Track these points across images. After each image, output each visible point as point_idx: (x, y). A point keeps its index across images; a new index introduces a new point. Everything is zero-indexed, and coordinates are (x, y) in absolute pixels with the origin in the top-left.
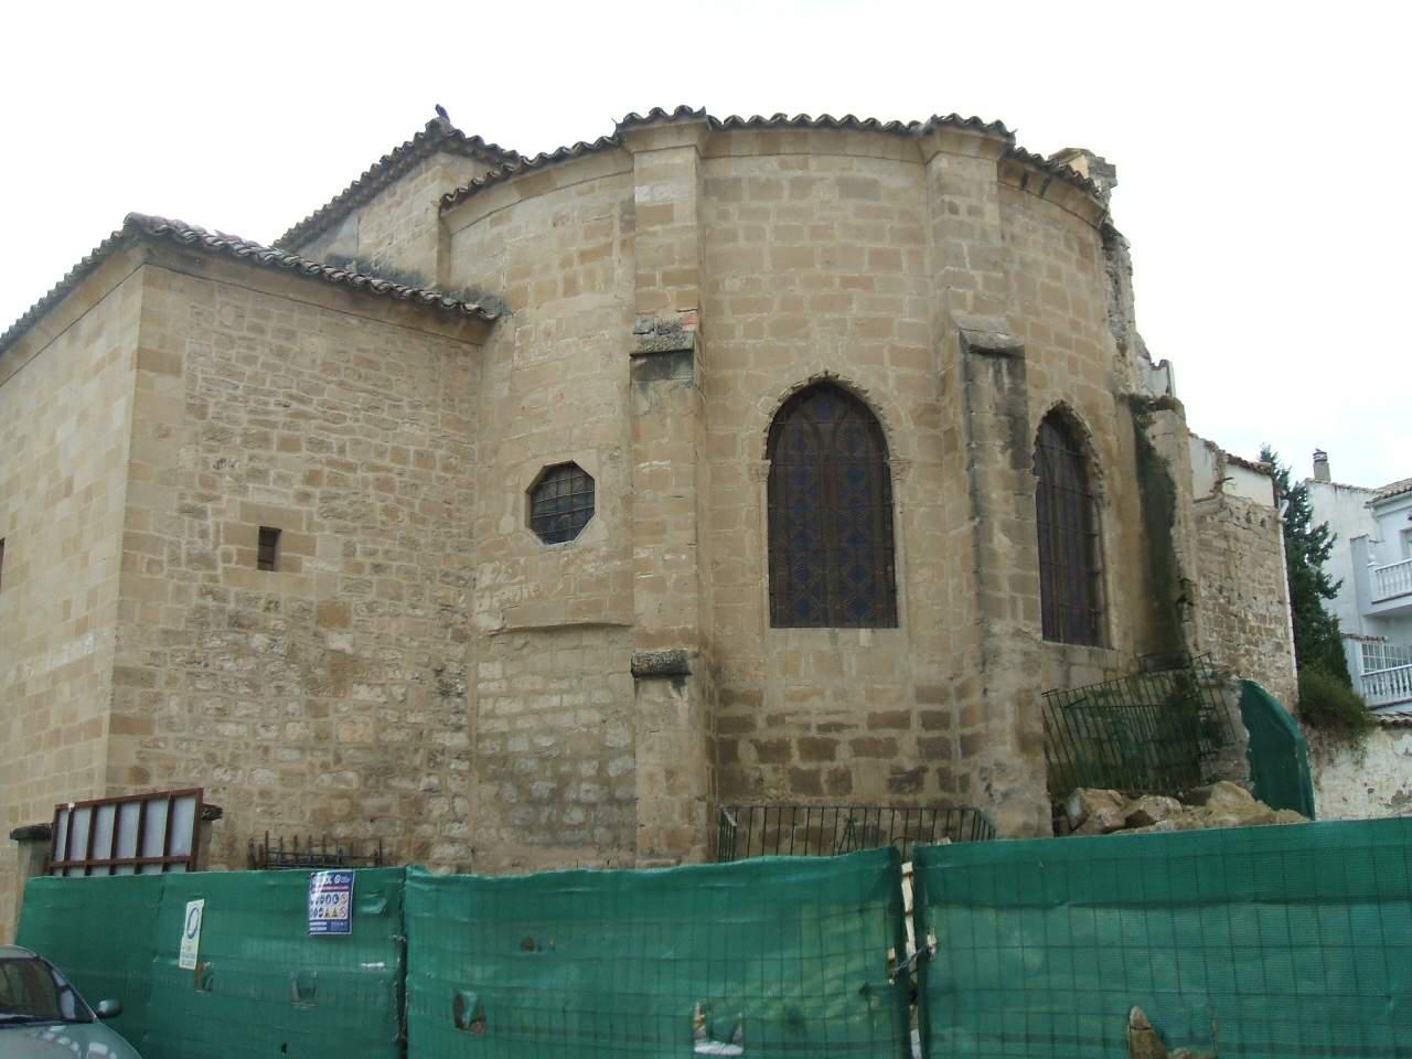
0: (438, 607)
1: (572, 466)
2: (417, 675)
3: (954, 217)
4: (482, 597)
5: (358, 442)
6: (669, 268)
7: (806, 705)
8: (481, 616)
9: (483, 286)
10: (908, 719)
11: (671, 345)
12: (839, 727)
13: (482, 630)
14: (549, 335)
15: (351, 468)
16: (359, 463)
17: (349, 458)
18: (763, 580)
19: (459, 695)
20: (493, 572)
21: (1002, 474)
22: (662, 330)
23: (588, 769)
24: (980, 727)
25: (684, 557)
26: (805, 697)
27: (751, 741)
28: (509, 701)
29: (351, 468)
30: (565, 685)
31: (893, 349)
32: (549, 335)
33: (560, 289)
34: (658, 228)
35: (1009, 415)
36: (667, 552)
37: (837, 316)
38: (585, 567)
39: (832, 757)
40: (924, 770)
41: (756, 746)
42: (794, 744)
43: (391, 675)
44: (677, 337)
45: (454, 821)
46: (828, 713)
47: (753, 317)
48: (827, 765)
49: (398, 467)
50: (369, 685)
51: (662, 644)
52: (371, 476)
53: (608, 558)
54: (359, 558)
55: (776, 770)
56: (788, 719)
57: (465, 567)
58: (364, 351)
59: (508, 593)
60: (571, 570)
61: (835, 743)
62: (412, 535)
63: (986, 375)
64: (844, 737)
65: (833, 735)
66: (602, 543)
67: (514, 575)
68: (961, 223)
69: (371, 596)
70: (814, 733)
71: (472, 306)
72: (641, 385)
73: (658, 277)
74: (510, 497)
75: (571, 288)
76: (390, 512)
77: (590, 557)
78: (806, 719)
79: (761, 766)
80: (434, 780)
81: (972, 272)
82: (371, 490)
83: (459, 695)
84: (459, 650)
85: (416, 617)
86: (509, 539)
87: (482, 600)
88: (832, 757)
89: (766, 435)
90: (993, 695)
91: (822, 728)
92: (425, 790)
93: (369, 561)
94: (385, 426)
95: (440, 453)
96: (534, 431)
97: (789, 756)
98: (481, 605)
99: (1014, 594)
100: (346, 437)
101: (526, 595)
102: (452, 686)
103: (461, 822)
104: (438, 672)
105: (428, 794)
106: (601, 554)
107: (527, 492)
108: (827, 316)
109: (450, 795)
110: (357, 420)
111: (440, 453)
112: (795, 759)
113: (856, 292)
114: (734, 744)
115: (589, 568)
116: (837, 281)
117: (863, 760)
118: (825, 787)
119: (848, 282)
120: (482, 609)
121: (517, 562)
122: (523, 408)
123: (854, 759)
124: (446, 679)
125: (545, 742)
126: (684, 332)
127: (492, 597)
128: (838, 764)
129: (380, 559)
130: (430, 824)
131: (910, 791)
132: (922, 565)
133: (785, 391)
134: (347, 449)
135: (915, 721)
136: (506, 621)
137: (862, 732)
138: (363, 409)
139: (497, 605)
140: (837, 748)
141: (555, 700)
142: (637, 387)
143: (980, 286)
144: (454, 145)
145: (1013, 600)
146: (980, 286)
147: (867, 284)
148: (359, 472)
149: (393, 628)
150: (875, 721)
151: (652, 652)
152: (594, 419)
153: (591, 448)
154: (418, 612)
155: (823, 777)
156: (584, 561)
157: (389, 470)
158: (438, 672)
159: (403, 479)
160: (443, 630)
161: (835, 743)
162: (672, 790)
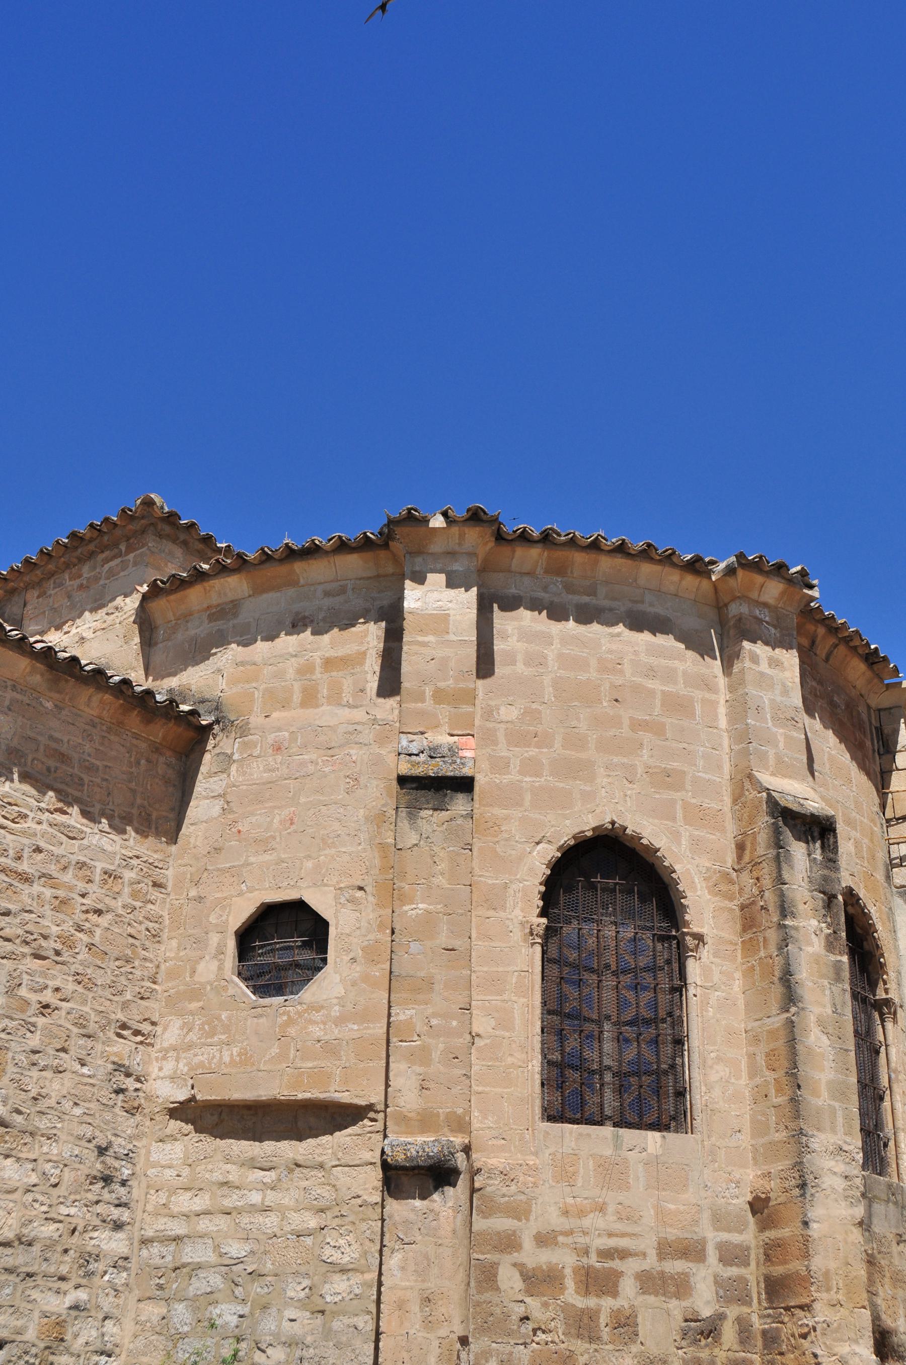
0: (110, 1067)
1: (300, 906)
2: (76, 1152)
3: (754, 667)
4: (165, 1058)
5: (38, 850)
6: (442, 685)
7: (586, 1222)
8: (159, 1082)
9: (193, 688)
10: (704, 1250)
11: (447, 770)
12: (623, 1254)
13: (160, 1100)
14: (279, 749)
15: (26, 879)
16: (37, 874)
17: (24, 866)
18: (535, 1062)
19: (124, 1183)
20: (182, 1028)
21: (817, 960)
22: (433, 753)
23: (295, 1291)
24: (796, 1266)
25: (454, 1023)
26: (582, 1213)
27: (515, 1265)
28: (189, 1194)
29: (26, 879)
30: (269, 1177)
31: (686, 806)
32: (279, 749)
33: (297, 697)
34: (431, 638)
35: (823, 893)
36: (435, 1015)
37: (625, 760)
38: (311, 1028)
39: (615, 1294)
40: (721, 1317)
41: (521, 1274)
42: (568, 1271)
43: (45, 1149)
44: (455, 762)
45: (102, 1354)
46: (610, 1235)
47: (532, 752)
48: (607, 1304)
49: (81, 886)
50: (18, 1159)
51: (423, 1131)
52: (48, 893)
53: (340, 1021)
54: (23, 992)
55: (545, 1305)
56: (561, 1239)
57: (145, 1020)
58: (57, 740)
59: (202, 1056)
60: (292, 1031)
61: (619, 1274)
62: (89, 971)
63: (798, 850)
64: (631, 1267)
65: (616, 1264)
66: (335, 1001)
67: (212, 1034)
68: (762, 674)
69: (34, 1041)
70: (593, 1260)
71: (185, 708)
72: (409, 813)
73: (428, 691)
74: (214, 939)
75: (310, 698)
76: (67, 941)
77: (317, 1016)
78: (582, 1240)
79: (528, 1300)
80: (82, 1295)
81: (775, 729)
82: (47, 911)
83: (124, 1183)
84: (128, 1125)
85: (83, 1075)
86: (209, 988)
87: (164, 1062)
88: (615, 1294)
89: (543, 888)
90: (814, 1226)
91: (606, 1254)
92: (70, 1308)
93: (33, 998)
94: (71, 834)
95: (129, 875)
96: (252, 859)
97: (562, 1288)
98: (160, 1069)
99: (832, 1103)
100: (26, 841)
101: (227, 1059)
102: (116, 1169)
103: (109, 1356)
104: (102, 1151)
105: (74, 1313)
106: (333, 1014)
107: (237, 933)
108: (616, 760)
109: (101, 1316)
110: (39, 823)
111: (129, 875)
112: (572, 1296)
113: (646, 737)
114: (494, 1266)
115: (317, 1031)
116: (626, 722)
117: (651, 1299)
118: (605, 1333)
119: (637, 725)
120: (161, 1074)
121: (218, 1018)
122: (239, 832)
123: (641, 1298)
124: (110, 1161)
125: (236, 1249)
126: (461, 758)
127: (177, 1060)
128: (620, 1302)
129: (48, 996)
130: (72, 1355)
131: (706, 1345)
132: (719, 1059)
133: (566, 838)
134: (26, 855)
135: (712, 1256)
136: (196, 1090)
137: (651, 1262)
138: (48, 810)
139: (186, 1069)
140: (621, 1280)
141: (255, 1198)
142: (404, 814)
143: (781, 745)
144: (167, 529)
145: (833, 1111)
146: (781, 745)
147: (658, 730)
148: (35, 885)
149: (56, 1087)
150: (665, 1250)
151: (410, 1140)
152: (333, 851)
153: (326, 885)
154: (85, 1070)
155: (603, 1319)
156: (312, 1022)
157: (71, 888)
158: (102, 1151)
159: (84, 901)
160: (113, 1096)
161: (619, 1274)
162: (428, 1323)
